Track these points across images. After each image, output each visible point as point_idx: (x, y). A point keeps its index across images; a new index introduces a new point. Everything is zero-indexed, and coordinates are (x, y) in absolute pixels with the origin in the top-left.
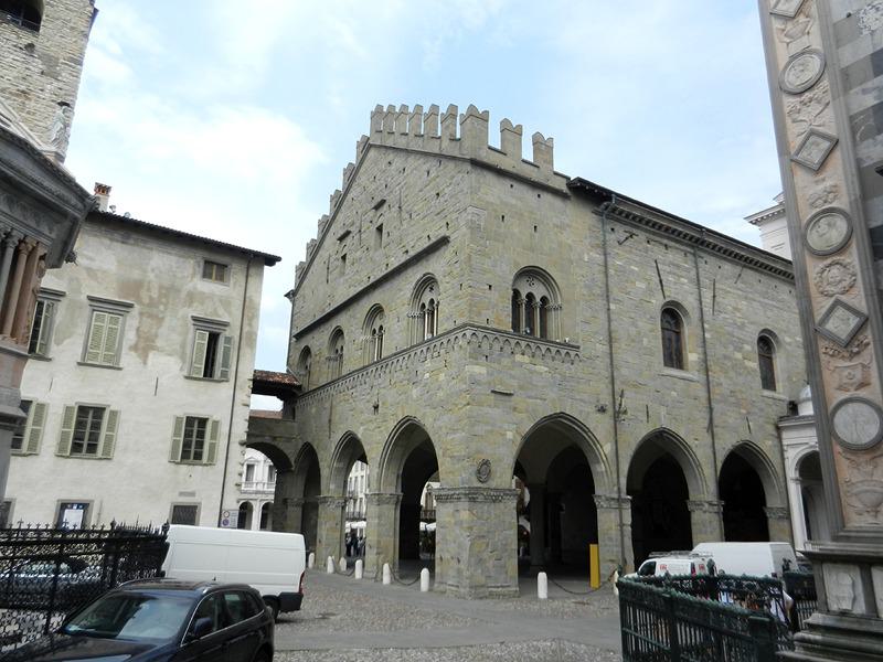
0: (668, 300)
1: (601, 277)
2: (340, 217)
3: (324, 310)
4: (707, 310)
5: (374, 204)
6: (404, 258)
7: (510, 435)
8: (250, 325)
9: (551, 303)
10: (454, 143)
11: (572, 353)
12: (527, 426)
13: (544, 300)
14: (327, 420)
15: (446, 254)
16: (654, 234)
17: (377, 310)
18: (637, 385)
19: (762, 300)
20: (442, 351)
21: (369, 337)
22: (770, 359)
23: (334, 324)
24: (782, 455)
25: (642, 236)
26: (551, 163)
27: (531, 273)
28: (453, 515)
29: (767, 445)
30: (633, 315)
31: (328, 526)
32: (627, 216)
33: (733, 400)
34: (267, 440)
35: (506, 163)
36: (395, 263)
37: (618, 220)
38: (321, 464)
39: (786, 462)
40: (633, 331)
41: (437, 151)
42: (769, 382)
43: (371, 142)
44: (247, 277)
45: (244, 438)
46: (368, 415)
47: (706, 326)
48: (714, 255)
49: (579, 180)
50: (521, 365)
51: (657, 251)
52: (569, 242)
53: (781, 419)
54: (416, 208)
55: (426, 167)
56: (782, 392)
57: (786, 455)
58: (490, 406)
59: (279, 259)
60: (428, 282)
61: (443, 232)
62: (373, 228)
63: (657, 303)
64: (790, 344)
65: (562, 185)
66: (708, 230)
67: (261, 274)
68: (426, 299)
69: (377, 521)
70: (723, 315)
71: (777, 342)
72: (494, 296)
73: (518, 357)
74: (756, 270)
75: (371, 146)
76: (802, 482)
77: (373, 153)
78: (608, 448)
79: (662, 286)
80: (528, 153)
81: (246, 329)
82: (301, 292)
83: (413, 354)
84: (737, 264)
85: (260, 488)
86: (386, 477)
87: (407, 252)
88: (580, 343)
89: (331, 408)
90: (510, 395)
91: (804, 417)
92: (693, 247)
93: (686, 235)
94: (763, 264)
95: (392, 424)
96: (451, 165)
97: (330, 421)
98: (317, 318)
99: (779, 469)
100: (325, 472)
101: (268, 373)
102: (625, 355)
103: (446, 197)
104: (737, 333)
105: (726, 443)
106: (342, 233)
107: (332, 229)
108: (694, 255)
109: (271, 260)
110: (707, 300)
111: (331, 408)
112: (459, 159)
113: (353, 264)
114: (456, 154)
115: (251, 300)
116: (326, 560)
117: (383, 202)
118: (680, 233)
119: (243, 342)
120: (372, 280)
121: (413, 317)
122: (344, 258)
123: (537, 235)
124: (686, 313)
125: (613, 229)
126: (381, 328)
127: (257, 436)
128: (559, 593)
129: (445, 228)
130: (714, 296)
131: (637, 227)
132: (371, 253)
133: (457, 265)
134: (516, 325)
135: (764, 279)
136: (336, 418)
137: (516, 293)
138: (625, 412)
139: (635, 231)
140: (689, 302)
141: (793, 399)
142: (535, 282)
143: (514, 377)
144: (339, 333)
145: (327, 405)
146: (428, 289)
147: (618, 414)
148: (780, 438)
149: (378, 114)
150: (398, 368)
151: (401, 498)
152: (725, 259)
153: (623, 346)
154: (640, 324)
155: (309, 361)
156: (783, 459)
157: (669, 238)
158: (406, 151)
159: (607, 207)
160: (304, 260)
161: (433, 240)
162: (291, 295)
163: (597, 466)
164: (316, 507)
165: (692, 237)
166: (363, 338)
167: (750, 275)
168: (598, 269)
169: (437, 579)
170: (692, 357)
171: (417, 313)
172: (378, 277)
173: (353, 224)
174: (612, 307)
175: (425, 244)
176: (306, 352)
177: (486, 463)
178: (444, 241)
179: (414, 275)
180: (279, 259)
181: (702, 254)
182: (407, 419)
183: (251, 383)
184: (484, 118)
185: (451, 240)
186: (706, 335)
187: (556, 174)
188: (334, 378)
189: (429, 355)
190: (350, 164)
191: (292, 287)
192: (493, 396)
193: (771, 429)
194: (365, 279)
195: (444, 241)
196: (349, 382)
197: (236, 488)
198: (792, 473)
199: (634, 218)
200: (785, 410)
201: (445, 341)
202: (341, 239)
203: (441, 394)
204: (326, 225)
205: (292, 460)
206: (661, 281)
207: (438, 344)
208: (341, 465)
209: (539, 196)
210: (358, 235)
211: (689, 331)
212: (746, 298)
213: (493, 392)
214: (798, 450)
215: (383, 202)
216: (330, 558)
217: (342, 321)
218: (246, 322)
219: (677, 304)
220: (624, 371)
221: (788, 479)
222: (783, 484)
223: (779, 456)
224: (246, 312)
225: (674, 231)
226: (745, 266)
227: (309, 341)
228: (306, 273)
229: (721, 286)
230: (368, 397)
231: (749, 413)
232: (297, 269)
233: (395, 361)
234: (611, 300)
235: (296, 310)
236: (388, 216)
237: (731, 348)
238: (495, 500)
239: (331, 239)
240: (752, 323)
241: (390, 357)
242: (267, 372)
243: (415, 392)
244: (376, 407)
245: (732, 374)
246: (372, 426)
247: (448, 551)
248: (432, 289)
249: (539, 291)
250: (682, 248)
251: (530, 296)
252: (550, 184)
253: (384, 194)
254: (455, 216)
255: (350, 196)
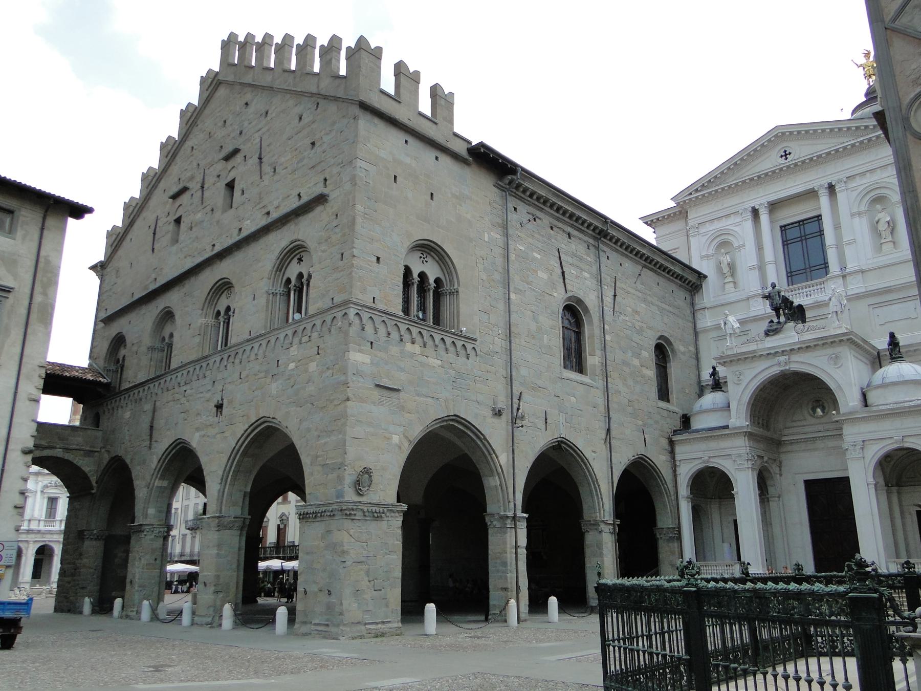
0: (569, 294)
1: (499, 261)
2: (175, 170)
3: (146, 287)
4: (608, 310)
5: (224, 153)
6: (264, 222)
7: (396, 439)
8: (45, 294)
9: (446, 287)
10: (337, 81)
11: (469, 346)
12: (417, 432)
13: (438, 281)
14: (145, 426)
15: (320, 214)
16: (558, 219)
17: (224, 287)
18: (536, 388)
19: (660, 304)
20: (315, 335)
21: (211, 320)
22: (665, 368)
23: (160, 304)
24: (675, 471)
25: (546, 220)
26: (451, 122)
27: (427, 248)
28: (323, 538)
29: (660, 460)
30: (533, 308)
31: (143, 561)
32: (531, 196)
33: (630, 409)
34: (58, 453)
35: (401, 113)
36: (250, 227)
37: (521, 199)
38: (137, 483)
39: (678, 479)
40: (533, 326)
41: (314, 89)
42: (664, 394)
43: (221, 78)
44: (42, 229)
45: (30, 444)
46: (208, 416)
47: (606, 327)
48: (617, 251)
49: (482, 145)
50: (412, 355)
51: (560, 241)
52: (469, 216)
53: (675, 432)
54: (283, 160)
55: (298, 110)
56: (676, 406)
57: (679, 471)
58: (374, 403)
59: (89, 210)
60: (296, 251)
61: (319, 189)
62: (222, 184)
63: (559, 298)
64: (684, 353)
65: (461, 149)
66: (613, 222)
67: (63, 230)
68: (293, 271)
69: (215, 551)
70: (622, 317)
71: (673, 351)
72: (382, 269)
73: (408, 346)
74: (655, 272)
75: (220, 83)
76: (692, 501)
77: (222, 92)
78: (503, 458)
79: (564, 279)
80: (425, 105)
81: (38, 298)
82: (114, 264)
83: (273, 340)
84: (637, 263)
85: (34, 526)
86: (230, 495)
87: (268, 213)
88: (477, 336)
89: (154, 411)
90: (397, 390)
91: (697, 431)
92: (595, 238)
93: (590, 225)
94: (661, 265)
95: (240, 428)
96: (332, 108)
97: (152, 427)
98: (136, 297)
99: (670, 485)
100: (141, 493)
101: (63, 367)
102: (524, 354)
103: (325, 146)
104: (636, 338)
105: (622, 461)
106: (175, 189)
107: (162, 185)
108: (597, 248)
109: (79, 211)
110: (608, 299)
111: (154, 411)
112: (344, 100)
113: (191, 228)
114: (340, 94)
115: (48, 262)
116: (140, 605)
117: (236, 151)
118: (584, 221)
119: (33, 316)
120: (218, 248)
121: (274, 294)
122: (178, 221)
123: (433, 203)
124: (586, 310)
125: (515, 209)
126: (228, 309)
127: (46, 448)
128: (450, 629)
129: (322, 184)
130: (615, 296)
131: (541, 210)
132: (218, 214)
133: (337, 230)
134: (406, 310)
135: (662, 281)
136: (160, 423)
137: (408, 271)
138: (523, 417)
139: (538, 213)
140: (591, 300)
141: (685, 412)
142: (429, 259)
143: (402, 370)
144: (168, 316)
145: (148, 407)
146: (295, 260)
147: (515, 420)
148: (672, 452)
149: (227, 45)
150: (253, 357)
151: (247, 522)
152: (627, 256)
153: (523, 343)
154: (541, 318)
155: (122, 352)
156: (675, 476)
157: (572, 226)
158: (271, 88)
159: (510, 183)
160: (137, 196)
161: (305, 199)
162: (99, 268)
163: (491, 479)
164: (127, 540)
165: (596, 228)
166: (202, 321)
167: (648, 275)
168: (498, 251)
169: (299, 618)
170: (592, 360)
171: (280, 289)
172: (226, 245)
173: (192, 178)
174: (513, 296)
175: (294, 204)
176: (119, 341)
177: (367, 471)
178: (321, 199)
179: (279, 241)
180: (89, 210)
181: (605, 248)
182: (261, 420)
183: (42, 382)
184: (377, 54)
185: (329, 199)
186: (608, 338)
187: (456, 135)
188: (158, 373)
189: (296, 340)
190: (169, 137)
191: (100, 256)
192: (377, 393)
193: (664, 443)
194: (209, 248)
195: (321, 199)
196: (180, 377)
197: (15, 511)
198: (684, 490)
199: (538, 199)
200: (678, 424)
201: (318, 322)
202: (175, 197)
203: (311, 388)
204: (151, 181)
205: (93, 479)
206: (563, 273)
207: (309, 326)
208: (165, 483)
209: (437, 158)
210: (200, 193)
211: (591, 332)
212: (645, 300)
213: (378, 386)
214: (692, 465)
215: (236, 151)
216: (146, 603)
217: (172, 299)
218: (38, 288)
219: (579, 301)
220: (524, 371)
221: (680, 497)
222: (674, 503)
223: (670, 471)
224: (39, 275)
225: (578, 218)
226: (644, 266)
227: (121, 326)
228: (174, 156)
229: (623, 286)
230: (208, 395)
231: (644, 425)
232: (109, 235)
233: (248, 348)
234: (512, 289)
235: (104, 297)
236: (242, 170)
237: (630, 354)
238: (377, 517)
239: (160, 197)
240: (650, 328)
241: (242, 343)
242: (60, 365)
243: (274, 387)
244: (219, 407)
245: (630, 382)
246: (212, 431)
247: (315, 582)
248: (300, 260)
249: (433, 272)
250: (586, 238)
251: (422, 275)
252: (449, 145)
253: (238, 144)
254: (335, 170)
255: (189, 144)
